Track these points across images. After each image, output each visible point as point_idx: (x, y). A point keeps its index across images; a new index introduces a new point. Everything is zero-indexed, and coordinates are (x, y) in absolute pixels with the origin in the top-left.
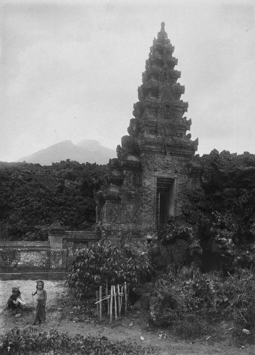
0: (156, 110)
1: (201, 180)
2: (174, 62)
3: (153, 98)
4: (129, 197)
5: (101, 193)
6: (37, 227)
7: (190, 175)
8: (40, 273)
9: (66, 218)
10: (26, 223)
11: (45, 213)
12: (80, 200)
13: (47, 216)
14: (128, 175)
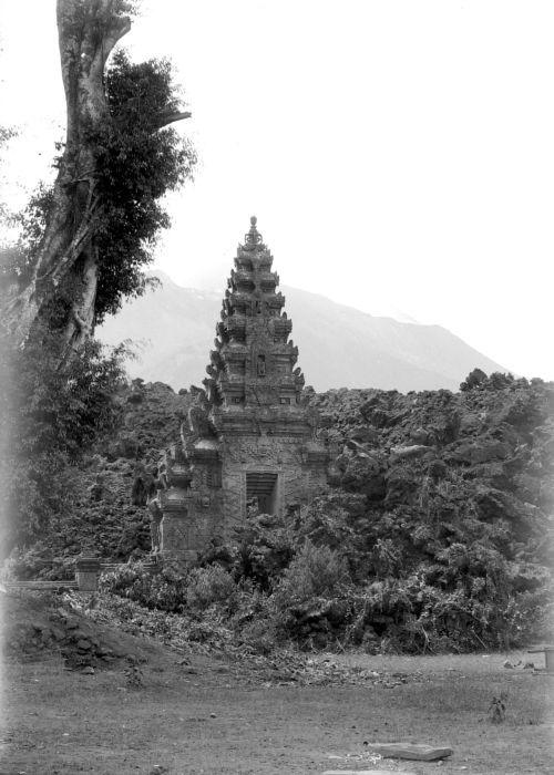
0: (242, 364)
1: (327, 473)
2: (272, 284)
3: (234, 345)
4: (201, 508)
5: (155, 503)
6: (56, 560)
7: (307, 465)
8: (68, 607)
9: (105, 545)
10: (38, 556)
11: (69, 538)
12: (131, 513)
13: (73, 543)
14: (197, 472)
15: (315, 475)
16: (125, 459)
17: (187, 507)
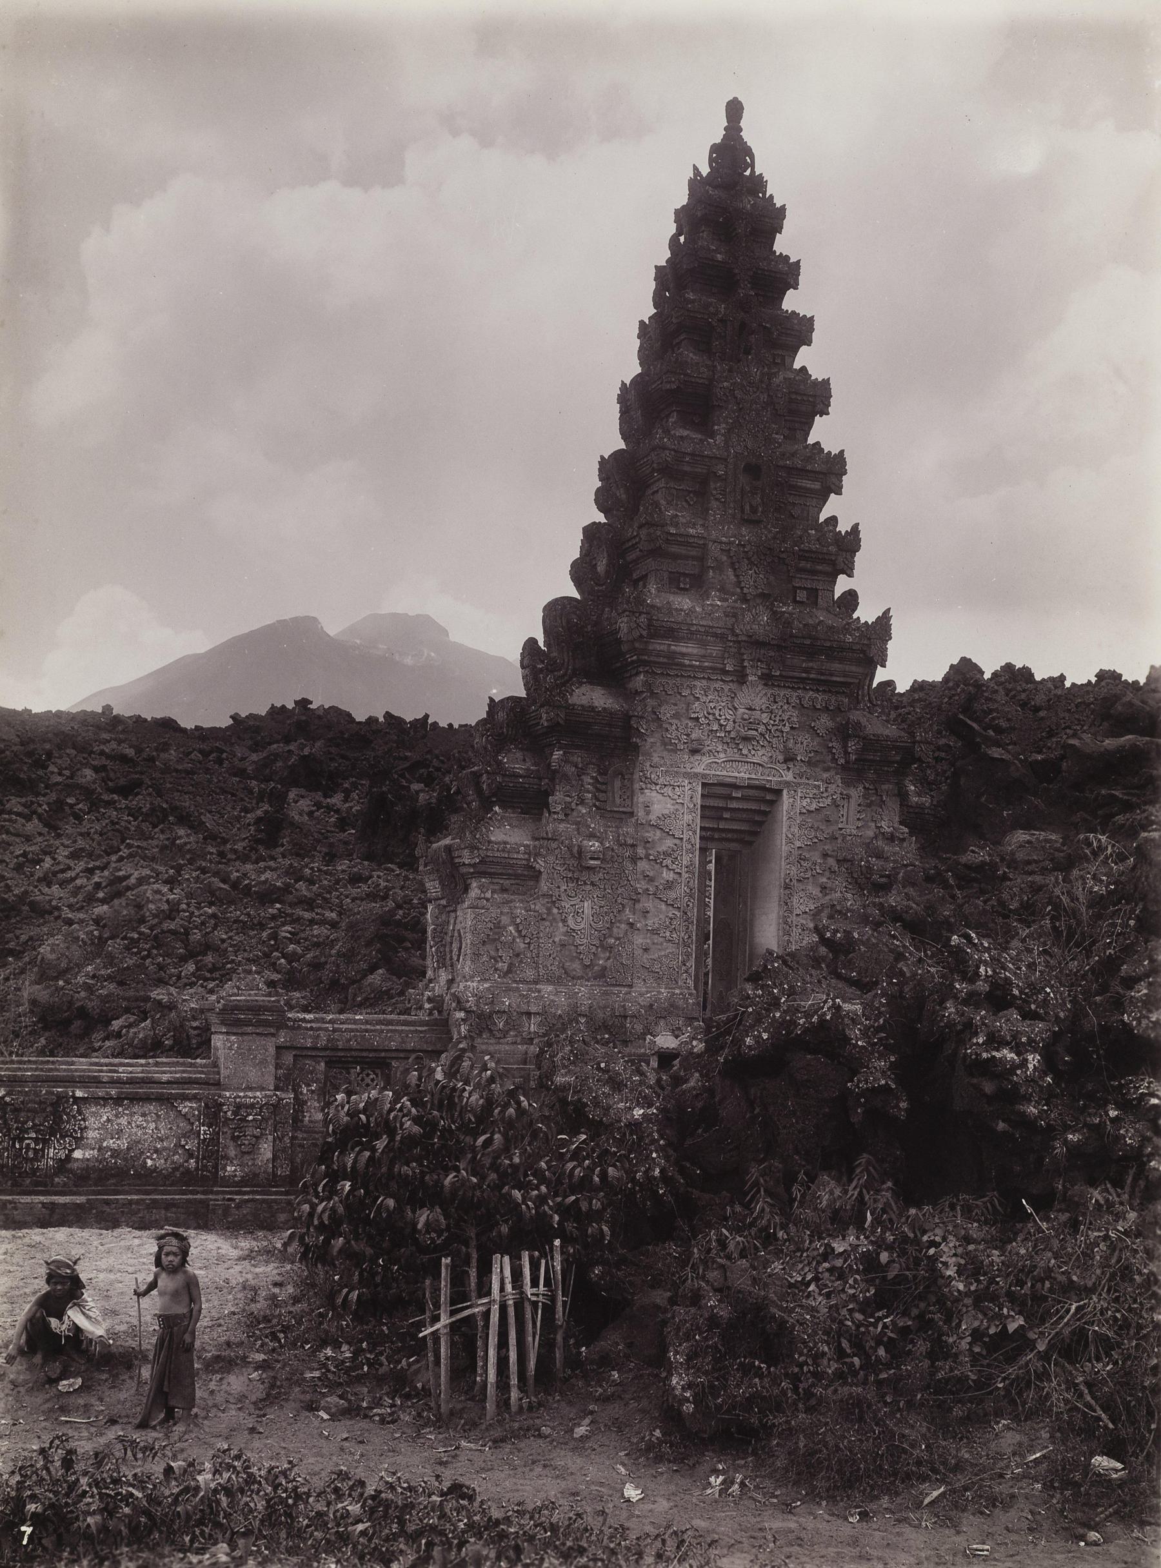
1: (903, 796)
6: (159, 994)
7: (853, 772)
9: (291, 958)
10: (110, 978)
11: (196, 936)
13: (207, 947)
15: (872, 803)
16: (303, 791)
17: (540, 864)
